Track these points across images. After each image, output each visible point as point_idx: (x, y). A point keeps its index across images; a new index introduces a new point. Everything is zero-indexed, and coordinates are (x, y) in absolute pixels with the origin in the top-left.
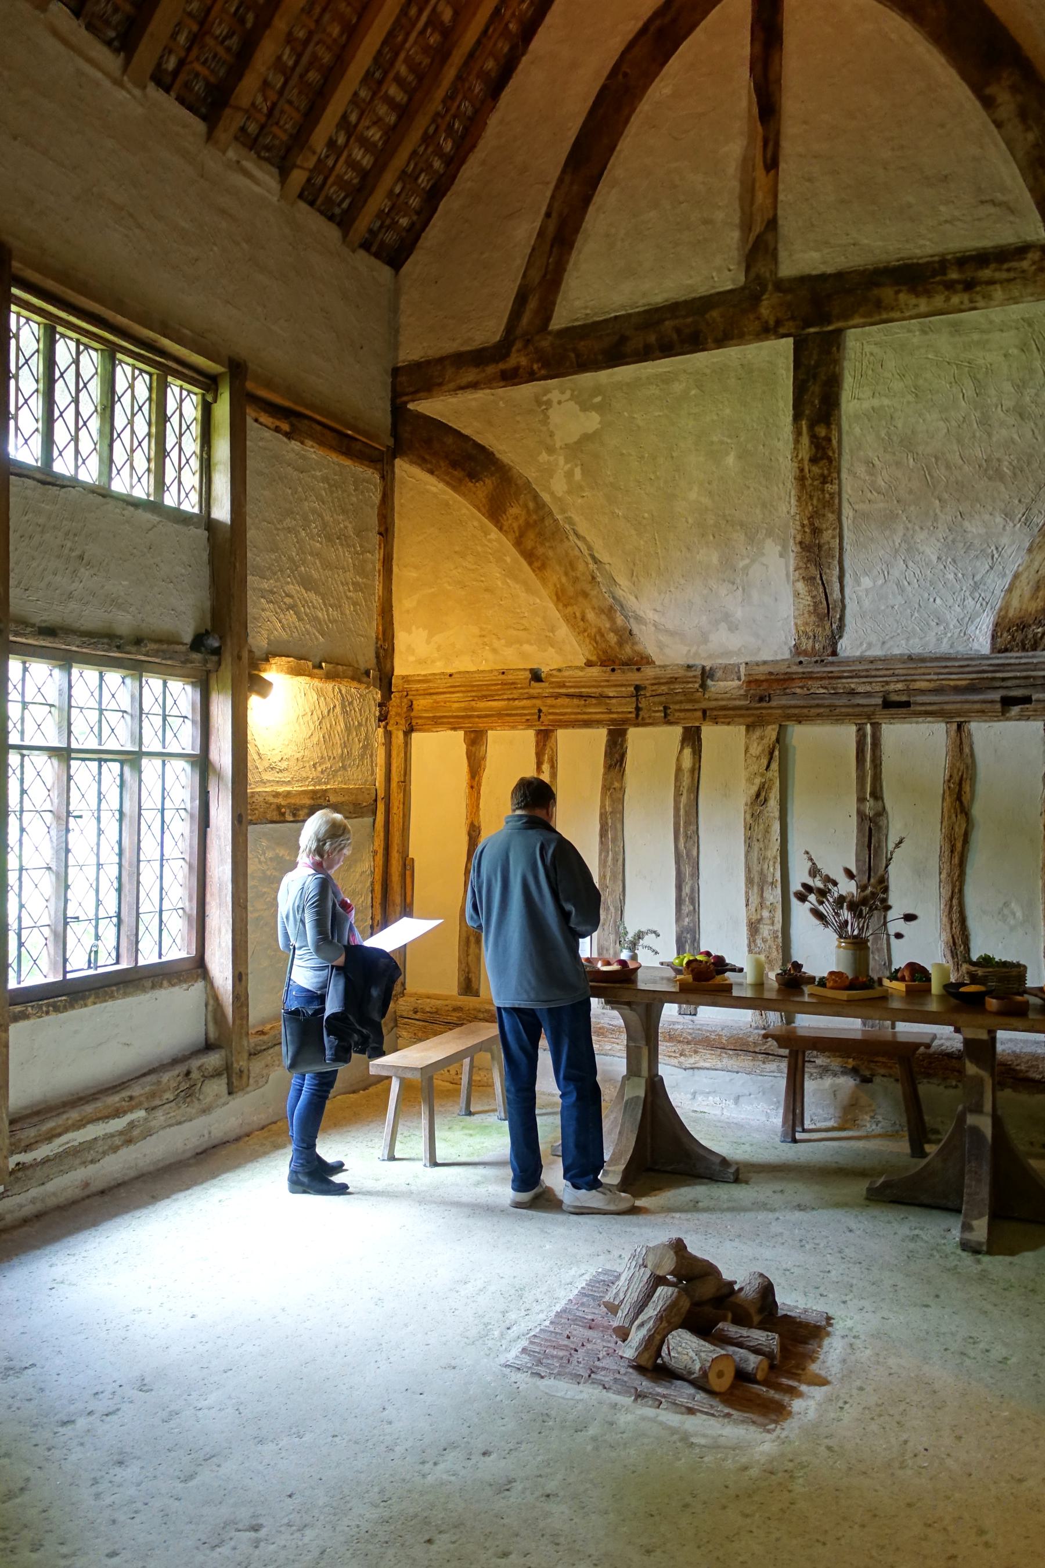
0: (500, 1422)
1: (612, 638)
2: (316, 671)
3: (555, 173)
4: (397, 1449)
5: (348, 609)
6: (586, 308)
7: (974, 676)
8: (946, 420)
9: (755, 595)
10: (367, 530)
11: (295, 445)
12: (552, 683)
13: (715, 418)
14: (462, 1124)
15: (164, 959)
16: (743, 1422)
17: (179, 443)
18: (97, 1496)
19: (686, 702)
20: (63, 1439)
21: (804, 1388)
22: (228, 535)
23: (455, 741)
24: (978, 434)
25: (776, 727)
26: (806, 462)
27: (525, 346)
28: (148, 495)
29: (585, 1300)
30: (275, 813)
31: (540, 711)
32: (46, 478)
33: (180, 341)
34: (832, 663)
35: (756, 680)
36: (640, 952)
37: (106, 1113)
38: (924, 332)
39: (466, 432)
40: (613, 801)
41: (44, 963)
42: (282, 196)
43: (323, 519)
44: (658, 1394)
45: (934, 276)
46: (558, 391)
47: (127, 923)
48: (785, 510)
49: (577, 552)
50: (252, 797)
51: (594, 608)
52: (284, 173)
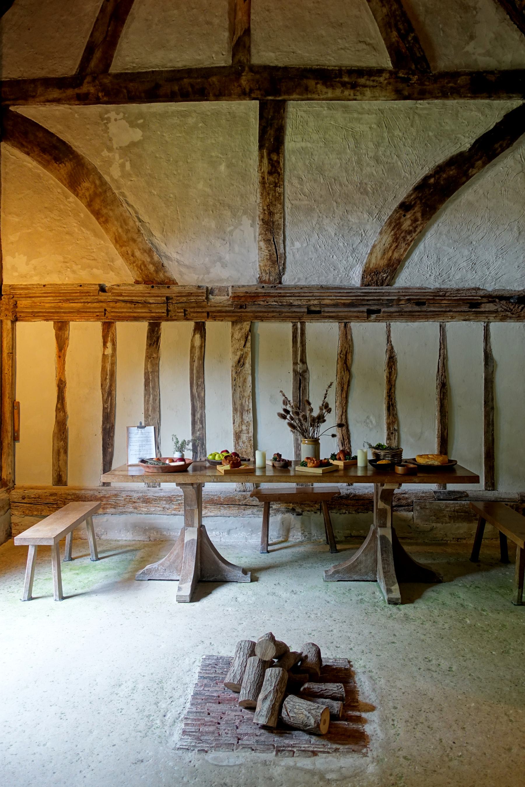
1: (152, 268)
6: (133, 63)
9: (237, 248)
14: (69, 567)
19: (197, 307)
23: (46, 329)
25: (249, 323)
26: (266, 174)
29: (205, 681)
31: (105, 310)
35: (238, 296)
49: (128, 214)
51: (140, 249)
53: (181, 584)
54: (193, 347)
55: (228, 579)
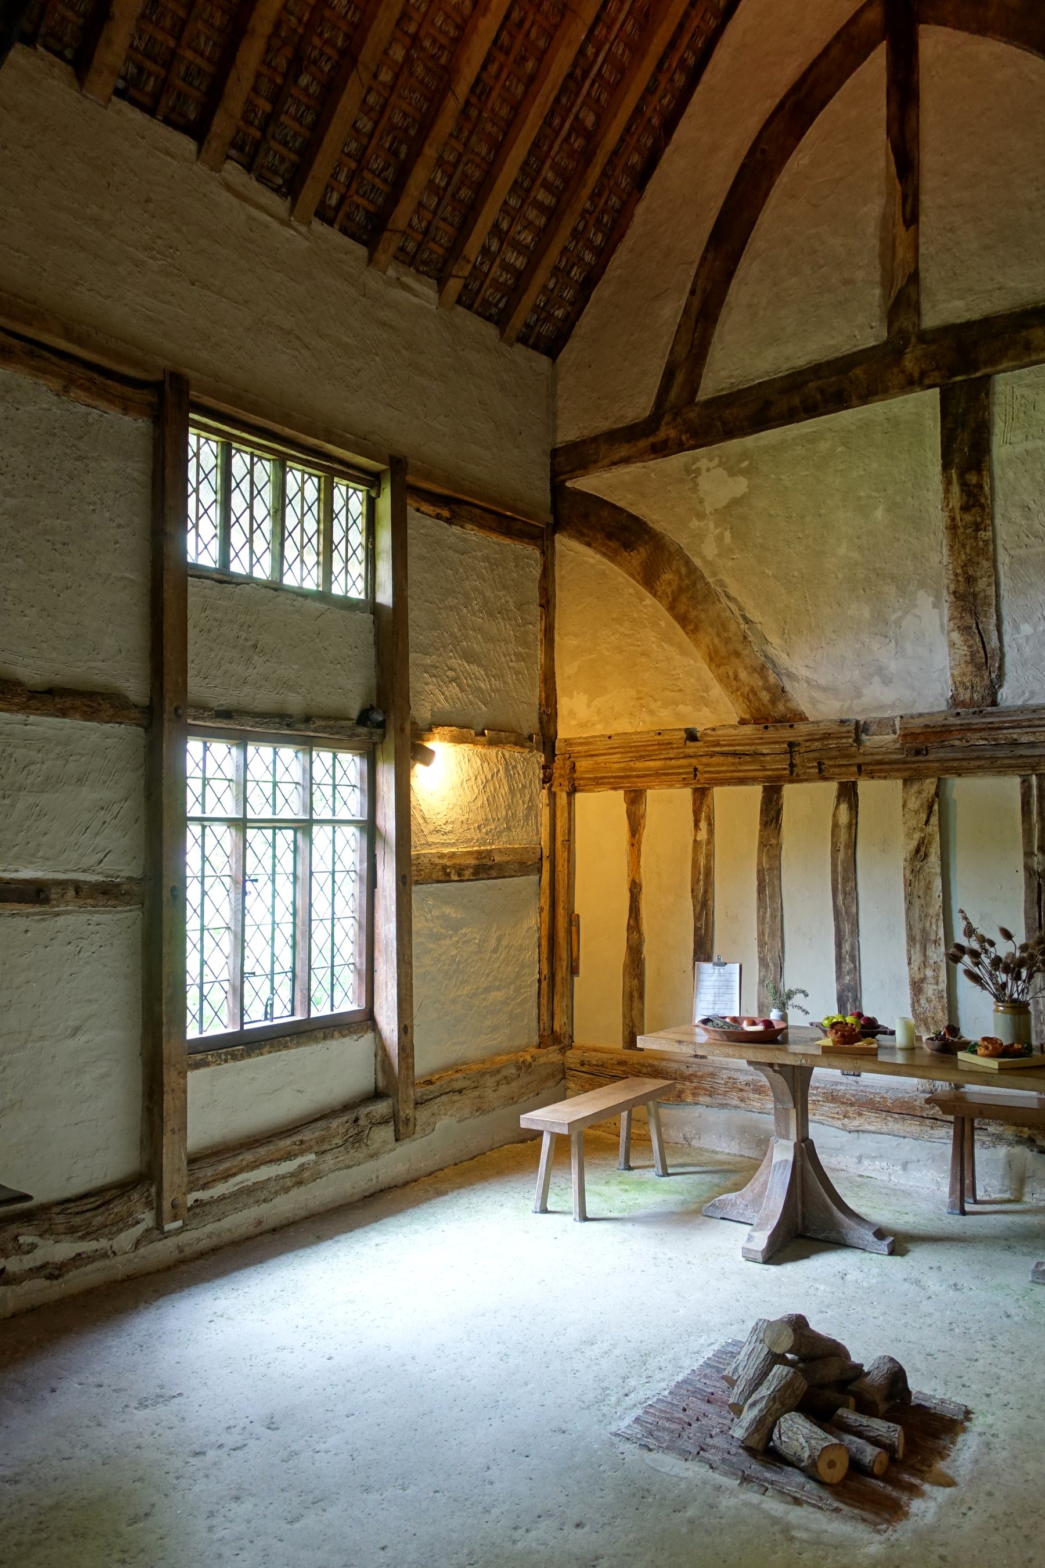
0: (599, 1493)
1: (765, 696)
2: (478, 738)
3: (697, 252)
4: (493, 1511)
5: (510, 678)
6: (731, 377)
9: (909, 647)
10: (528, 603)
11: (456, 529)
12: (708, 741)
13: (862, 473)
14: (620, 1179)
15: (336, 1011)
16: (852, 1518)
17: (346, 536)
18: (210, 1529)
19: (842, 756)
20: (192, 1469)
21: (926, 1487)
22: (391, 618)
23: (615, 800)
25: (934, 780)
26: (957, 511)
27: (674, 420)
28: (318, 586)
29: (708, 1371)
30: (440, 873)
31: (696, 769)
32: (223, 577)
34: (992, 714)
35: (912, 734)
36: (790, 1011)
37: (278, 1155)
40: (770, 858)
41: (224, 1014)
42: (441, 304)
43: (484, 596)
44: (766, 1480)
46: (706, 460)
47: (301, 977)
48: (937, 560)
49: (728, 613)
50: (418, 858)
51: (746, 668)
52: (441, 283)
53: (754, 1230)
54: (835, 826)
55: (849, 1242)
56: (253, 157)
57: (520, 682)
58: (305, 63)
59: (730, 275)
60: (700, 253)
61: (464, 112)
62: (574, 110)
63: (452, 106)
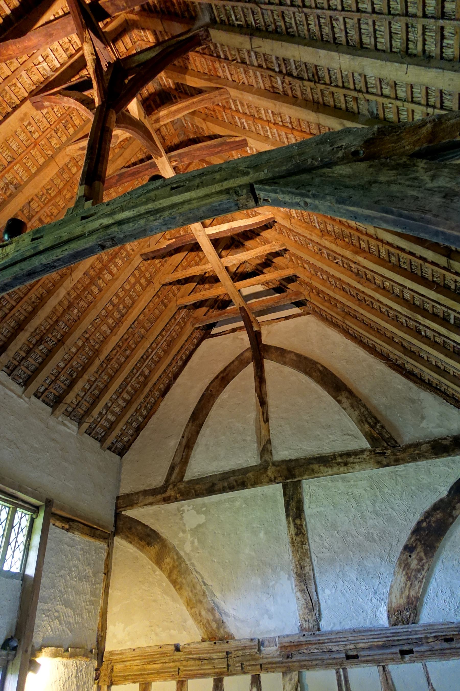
1: (214, 625)
2: (65, 653)
5: (85, 615)
7: (384, 639)
8: (348, 517)
11: (70, 534)
22: (32, 583)
24: (361, 522)
25: (297, 673)
26: (294, 535)
27: (174, 488)
31: (179, 669)
33: (26, 493)
34: (319, 635)
35: (284, 646)
38: (332, 481)
39: (146, 524)
45: (332, 460)
46: (187, 506)
49: (196, 580)
51: (205, 609)
52: (80, 424)
56: (12, 371)
57: (90, 618)
58: (43, 342)
59: (198, 432)
60: (186, 423)
61: (101, 365)
62: (142, 368)
63: (97, 362)
